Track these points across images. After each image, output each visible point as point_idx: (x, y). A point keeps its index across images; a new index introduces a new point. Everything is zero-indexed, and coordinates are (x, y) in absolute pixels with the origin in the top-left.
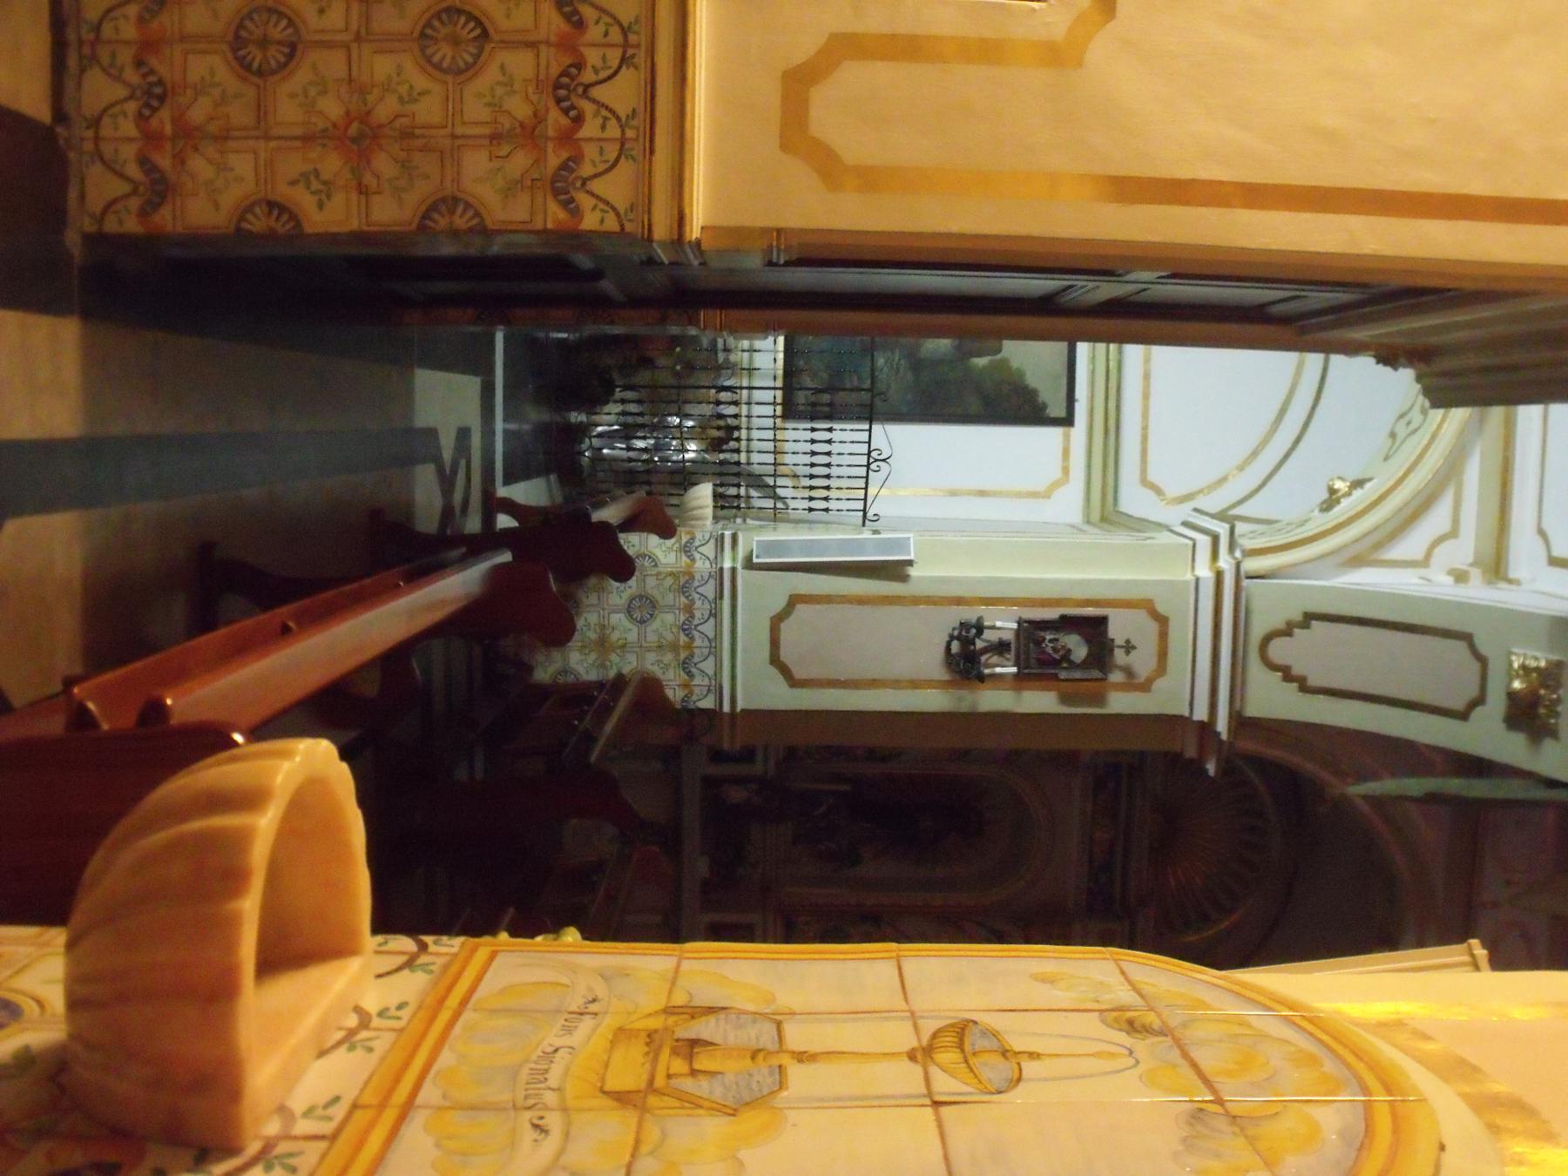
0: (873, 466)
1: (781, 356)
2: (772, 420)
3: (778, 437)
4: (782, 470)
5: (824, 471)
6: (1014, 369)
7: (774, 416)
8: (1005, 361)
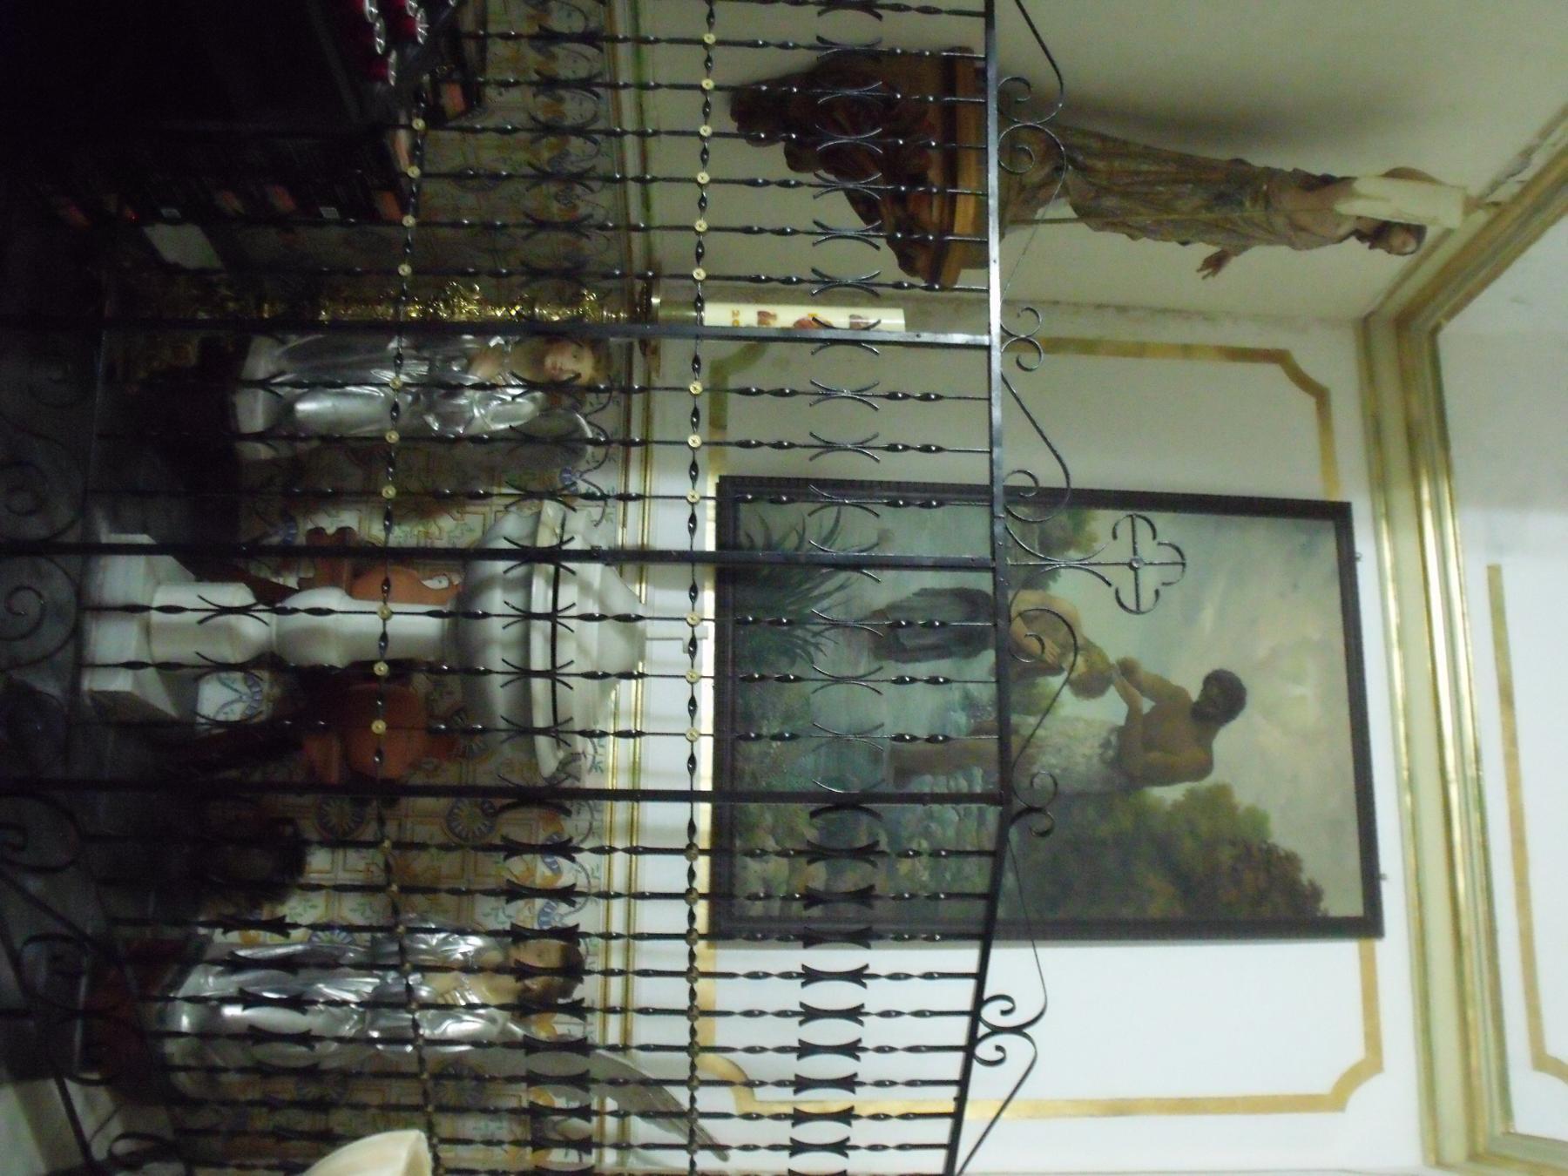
0: (985, 1050)
1: (706, 751)
2: (682, 946)
3: (701, 965)
4: (711, 1065)
5: (840, 1066)
6: (1242, 808)
7: (689, 936)
8: (1219, 799)
